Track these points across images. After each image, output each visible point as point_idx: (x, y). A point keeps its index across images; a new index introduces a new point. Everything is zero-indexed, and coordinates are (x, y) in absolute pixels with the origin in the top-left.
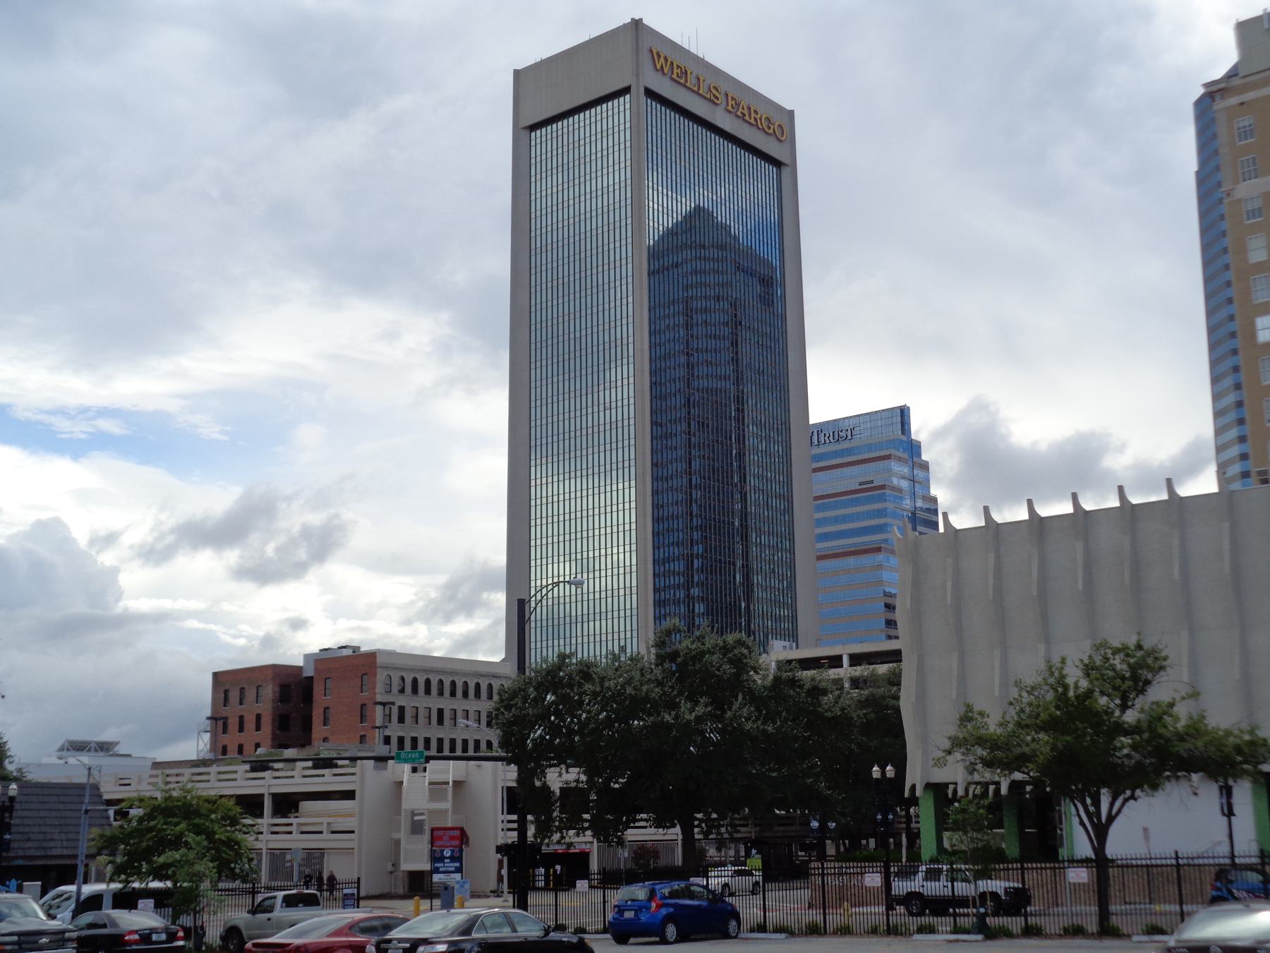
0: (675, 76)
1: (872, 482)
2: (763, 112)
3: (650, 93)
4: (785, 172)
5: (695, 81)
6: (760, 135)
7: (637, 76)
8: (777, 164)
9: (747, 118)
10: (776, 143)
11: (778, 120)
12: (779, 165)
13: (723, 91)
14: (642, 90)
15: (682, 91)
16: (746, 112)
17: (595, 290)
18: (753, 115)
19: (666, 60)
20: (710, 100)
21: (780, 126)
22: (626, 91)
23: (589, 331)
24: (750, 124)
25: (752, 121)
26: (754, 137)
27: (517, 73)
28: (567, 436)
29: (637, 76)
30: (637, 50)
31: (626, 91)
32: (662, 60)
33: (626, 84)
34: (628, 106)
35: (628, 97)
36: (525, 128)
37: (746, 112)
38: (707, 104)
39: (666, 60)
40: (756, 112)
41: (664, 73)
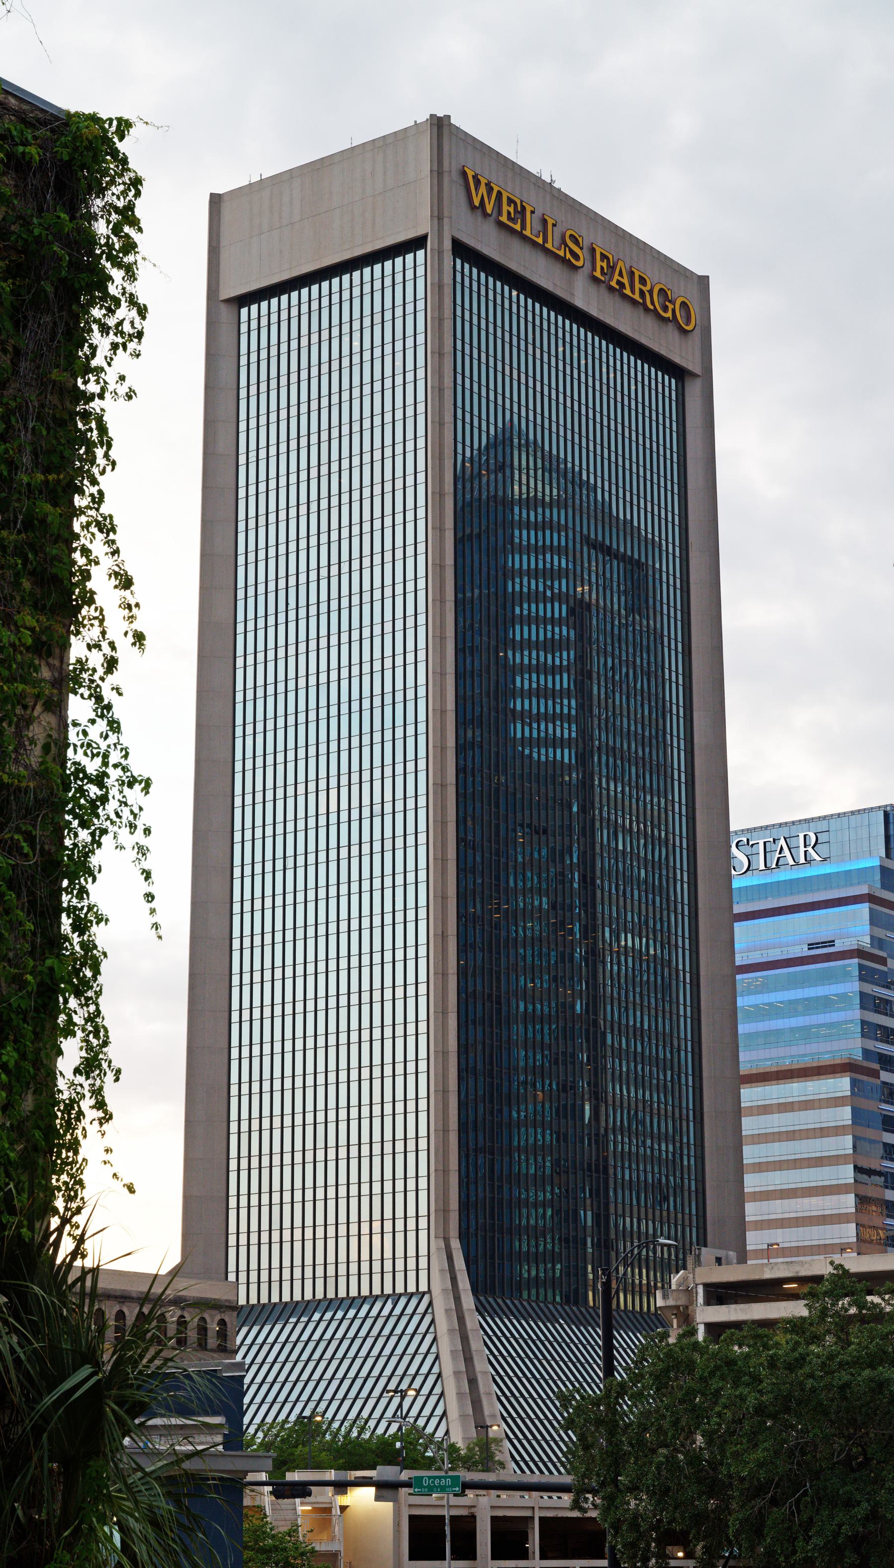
0: (504, 219)
1: (831, 943)
2: (656, 278)
3: (460, 249)
4: (693, 390)
5: (538, 227)
6: (649, 322)
7: (440, 219)
8: (679, 373)
9: (628, 291)
10: (676, 334)
11: (681, 292)
12: (685, 379)
13: (586, 244)
14: (448, 245)
15: (516, 245)
16: (625, 281)
17: (356, 600)
18: (637, 286)
19: (490, 189)
20: (564, 261)
21: (684, 304)
22: (418, 243)
23: (261, 623)
24: (634, 302)
25: (637, 297)
26: (644, 328)
27: (216, 200)
28: (311, 858)
29: (440, 219)
30: (438, 173)
31: (418, 243)
32: (483, 189)
33: (420, 232)
34: (420, 271)
35: (420, 254)
36: (228, 301)
37: (625, 281)
38: (558, 270)
39: (490, 189)
40: (643, 281)
41: (485, 215)
